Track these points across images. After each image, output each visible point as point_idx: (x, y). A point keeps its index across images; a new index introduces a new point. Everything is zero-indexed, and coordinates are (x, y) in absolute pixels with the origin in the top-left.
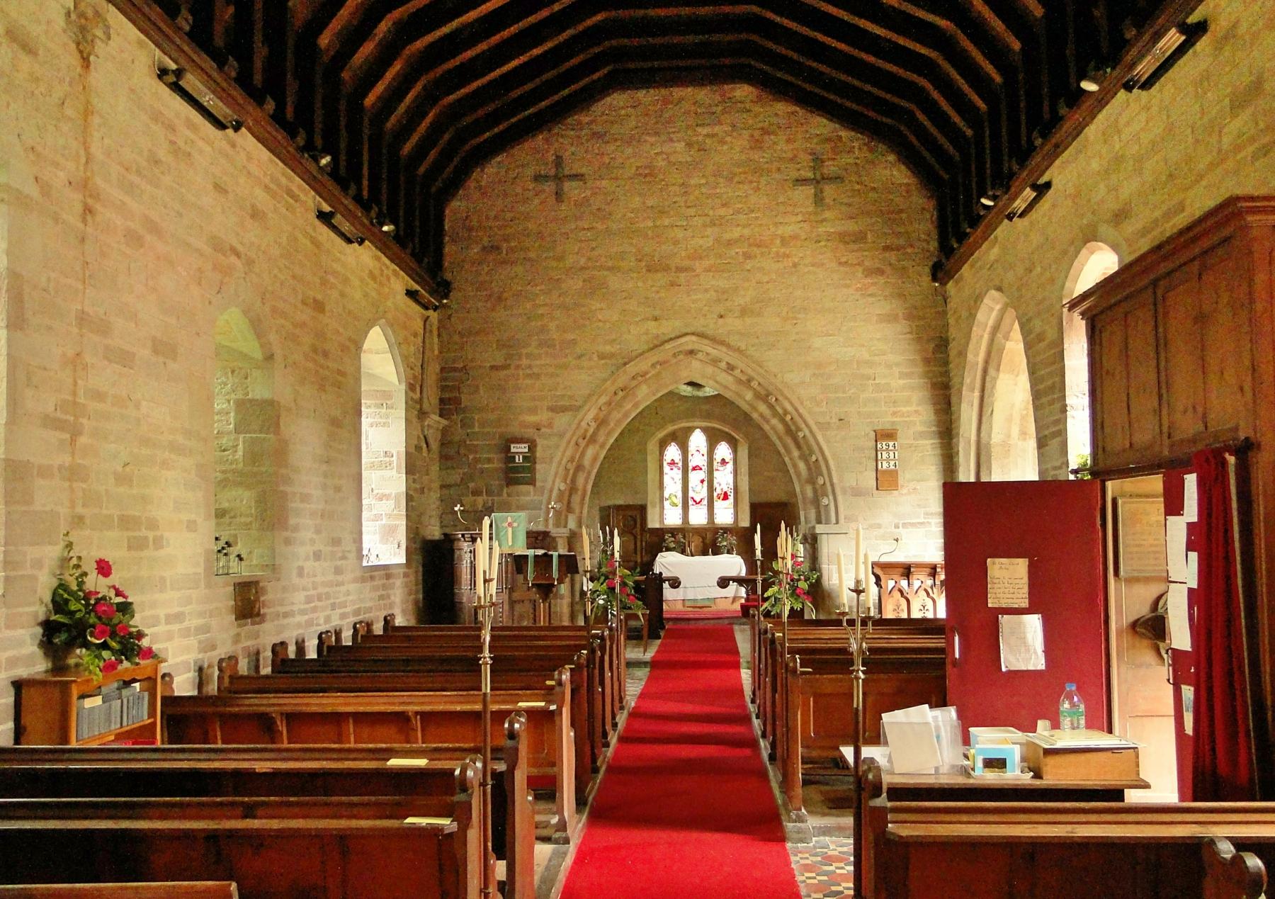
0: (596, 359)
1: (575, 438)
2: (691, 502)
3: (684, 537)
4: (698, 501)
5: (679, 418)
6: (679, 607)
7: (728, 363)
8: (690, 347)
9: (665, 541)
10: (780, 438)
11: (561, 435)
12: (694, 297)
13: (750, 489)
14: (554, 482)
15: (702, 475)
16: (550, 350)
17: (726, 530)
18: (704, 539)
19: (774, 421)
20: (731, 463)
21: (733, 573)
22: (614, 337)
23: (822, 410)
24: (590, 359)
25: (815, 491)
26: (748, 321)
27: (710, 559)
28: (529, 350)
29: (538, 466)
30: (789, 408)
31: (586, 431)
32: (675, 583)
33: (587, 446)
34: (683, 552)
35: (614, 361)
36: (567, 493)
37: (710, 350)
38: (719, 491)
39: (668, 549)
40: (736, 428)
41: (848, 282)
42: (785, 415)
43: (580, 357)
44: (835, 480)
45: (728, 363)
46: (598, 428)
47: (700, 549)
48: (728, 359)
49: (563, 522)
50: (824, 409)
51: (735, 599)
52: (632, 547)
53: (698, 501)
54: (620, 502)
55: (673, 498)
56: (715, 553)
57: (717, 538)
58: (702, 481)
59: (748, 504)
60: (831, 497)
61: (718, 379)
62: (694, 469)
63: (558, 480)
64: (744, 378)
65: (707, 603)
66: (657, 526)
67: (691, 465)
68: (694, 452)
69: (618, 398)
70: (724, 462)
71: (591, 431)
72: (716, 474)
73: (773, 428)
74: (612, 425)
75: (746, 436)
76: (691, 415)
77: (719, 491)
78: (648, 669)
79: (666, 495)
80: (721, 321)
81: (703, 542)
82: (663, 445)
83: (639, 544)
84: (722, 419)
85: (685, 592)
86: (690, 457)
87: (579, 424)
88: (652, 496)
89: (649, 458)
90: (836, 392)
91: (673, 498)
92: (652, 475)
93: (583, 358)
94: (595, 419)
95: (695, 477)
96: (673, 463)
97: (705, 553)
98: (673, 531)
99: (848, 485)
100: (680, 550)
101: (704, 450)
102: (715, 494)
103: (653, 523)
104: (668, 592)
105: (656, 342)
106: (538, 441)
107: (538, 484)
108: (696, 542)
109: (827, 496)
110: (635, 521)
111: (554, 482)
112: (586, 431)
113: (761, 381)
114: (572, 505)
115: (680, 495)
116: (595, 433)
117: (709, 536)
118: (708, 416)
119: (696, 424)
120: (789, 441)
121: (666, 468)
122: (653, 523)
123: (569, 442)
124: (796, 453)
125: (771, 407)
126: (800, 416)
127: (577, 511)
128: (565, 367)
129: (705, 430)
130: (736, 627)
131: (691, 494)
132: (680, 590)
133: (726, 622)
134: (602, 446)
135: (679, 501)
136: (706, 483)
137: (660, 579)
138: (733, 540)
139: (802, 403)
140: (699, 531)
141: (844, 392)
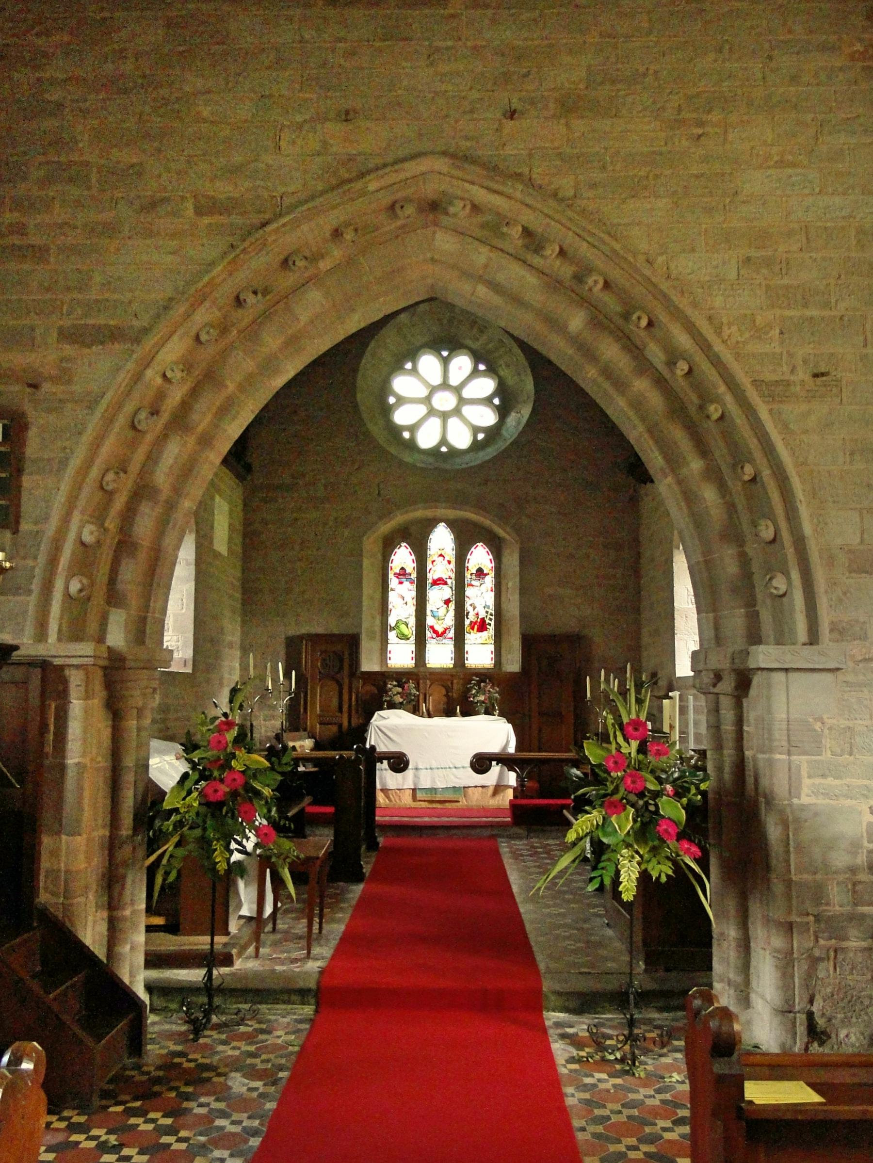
0: (190, 212)
1: (129, 408)
2: (429, 634)
3: (417, 688)
4: (440, 630)
5: (411, 501)
6: (407, 800)
7: (527, 232)
8: (431, 189)
9: (386, 692)
10: (652, 430)
11: (92, 403)
12: (443, 68)
13: (521, 615)
14: (66, 520)
15: (446, 592)
16: (74, 192)
17: (483, 676)
18: (448, 690)
19: (641, 385)
20: (492, 574)
21: (493, 747)
22: (238, 159)
23: (767, 348)
24: (175, 214)
25: (744, 560)
26: (579, 126)
27: (457, 722)
28: (22, 189)
29: (27, 481)
30: (683, 340)
31: (161, 396)
32: (399, 763)
33: (163, 438)
34: (415, 711)
35: (236, 219)
36: (106, 556)
37: (480, 194)
38: (472, 617)
39: (392, 706)
40: (503, 518)
41: (833, 38)
42: (671, 363)
43: (152, 205)
44: (807, 529)
45: (527, 232)
46: (194, 393)
47: (442, 706)
48: (528, 218)
49: (92, 627)
50: (775, 347)
51: (499, 788)
52: (335, 702)
53: (440, 630)
54: (319, 629)
55: (403, 628)
56: (466, 713)
57: (470, 690)
58: (447, 602)
59: (143, 984)
60: (795, 575)
61: (501, 278)
62: (435, 583)
63: (76, 518)
64: (566, 271)
65: (449, 796)
66: (376, 668)
67: (431, 576)
68: (435, 558)
69: (245, 317)
70: (480, 573)
71: (176, 396)
72: (469, 591)
73: (637, 404)
74: (231, 387)
75: (518, 530)
76: (432, 499)
77: (472, 617)
78: (308, 1010)
79: (392, 621)
80: (509, 125)
81: (447, 695)
82: (389, 546)
83: (346, 697)
84: (480, 506)
85: (416, 777)
86: (429, 566)
87: (138, 377)
88: (368, 622)
89: (366, 562)
90: (805, 306)
91: (403, 628)
92: (369, 588)
93: (162, 210)
94: (188, 366)
95: (437, 596)
96: (402, 574)
97: (449, 712)
98: (401, 677)
99: (839, 541)
100: (410, 706)
101: (451, 554)
102: (467, 622)
103: (369, 664)
104: (385, 776)
105: (344, 174)
106: (31, 413)
107: (25, 526)
108: (436, 696)
109: (786, 574)
110: (341, 661)
111: (66, 520)
112: (161, 396)
113: (616, 274)
114: (120, 586)
115: (412, 622)
116: (185, 407)
117: (457, 686)
118: (459, 500)
119: (440, 512)
120: (679, 435)
121: (393, 582)
122: (369, 664)
123: (109, 420)
124: (696, 465)
125: (634, 349)
126: (717, 362)
127: (134, 602)
128: (110, 229)
129: (452, 525)
130: (504, 848)
131: (430, 621)
132: (409, 773)
133: (487, 833)
134: (206, 441)
135: (410, 631)
136: (452, 606)
137: (372, 757)
138: (495, 693)
139: (718, 332)
140: (440, 677)
141: (827, 305)
